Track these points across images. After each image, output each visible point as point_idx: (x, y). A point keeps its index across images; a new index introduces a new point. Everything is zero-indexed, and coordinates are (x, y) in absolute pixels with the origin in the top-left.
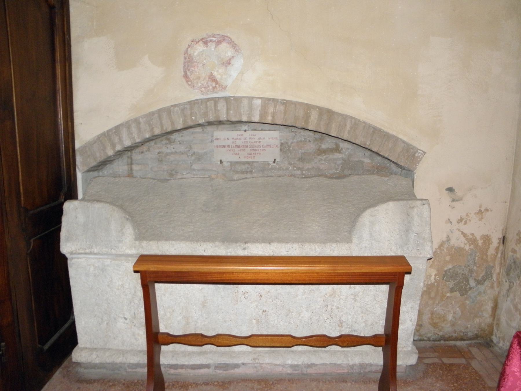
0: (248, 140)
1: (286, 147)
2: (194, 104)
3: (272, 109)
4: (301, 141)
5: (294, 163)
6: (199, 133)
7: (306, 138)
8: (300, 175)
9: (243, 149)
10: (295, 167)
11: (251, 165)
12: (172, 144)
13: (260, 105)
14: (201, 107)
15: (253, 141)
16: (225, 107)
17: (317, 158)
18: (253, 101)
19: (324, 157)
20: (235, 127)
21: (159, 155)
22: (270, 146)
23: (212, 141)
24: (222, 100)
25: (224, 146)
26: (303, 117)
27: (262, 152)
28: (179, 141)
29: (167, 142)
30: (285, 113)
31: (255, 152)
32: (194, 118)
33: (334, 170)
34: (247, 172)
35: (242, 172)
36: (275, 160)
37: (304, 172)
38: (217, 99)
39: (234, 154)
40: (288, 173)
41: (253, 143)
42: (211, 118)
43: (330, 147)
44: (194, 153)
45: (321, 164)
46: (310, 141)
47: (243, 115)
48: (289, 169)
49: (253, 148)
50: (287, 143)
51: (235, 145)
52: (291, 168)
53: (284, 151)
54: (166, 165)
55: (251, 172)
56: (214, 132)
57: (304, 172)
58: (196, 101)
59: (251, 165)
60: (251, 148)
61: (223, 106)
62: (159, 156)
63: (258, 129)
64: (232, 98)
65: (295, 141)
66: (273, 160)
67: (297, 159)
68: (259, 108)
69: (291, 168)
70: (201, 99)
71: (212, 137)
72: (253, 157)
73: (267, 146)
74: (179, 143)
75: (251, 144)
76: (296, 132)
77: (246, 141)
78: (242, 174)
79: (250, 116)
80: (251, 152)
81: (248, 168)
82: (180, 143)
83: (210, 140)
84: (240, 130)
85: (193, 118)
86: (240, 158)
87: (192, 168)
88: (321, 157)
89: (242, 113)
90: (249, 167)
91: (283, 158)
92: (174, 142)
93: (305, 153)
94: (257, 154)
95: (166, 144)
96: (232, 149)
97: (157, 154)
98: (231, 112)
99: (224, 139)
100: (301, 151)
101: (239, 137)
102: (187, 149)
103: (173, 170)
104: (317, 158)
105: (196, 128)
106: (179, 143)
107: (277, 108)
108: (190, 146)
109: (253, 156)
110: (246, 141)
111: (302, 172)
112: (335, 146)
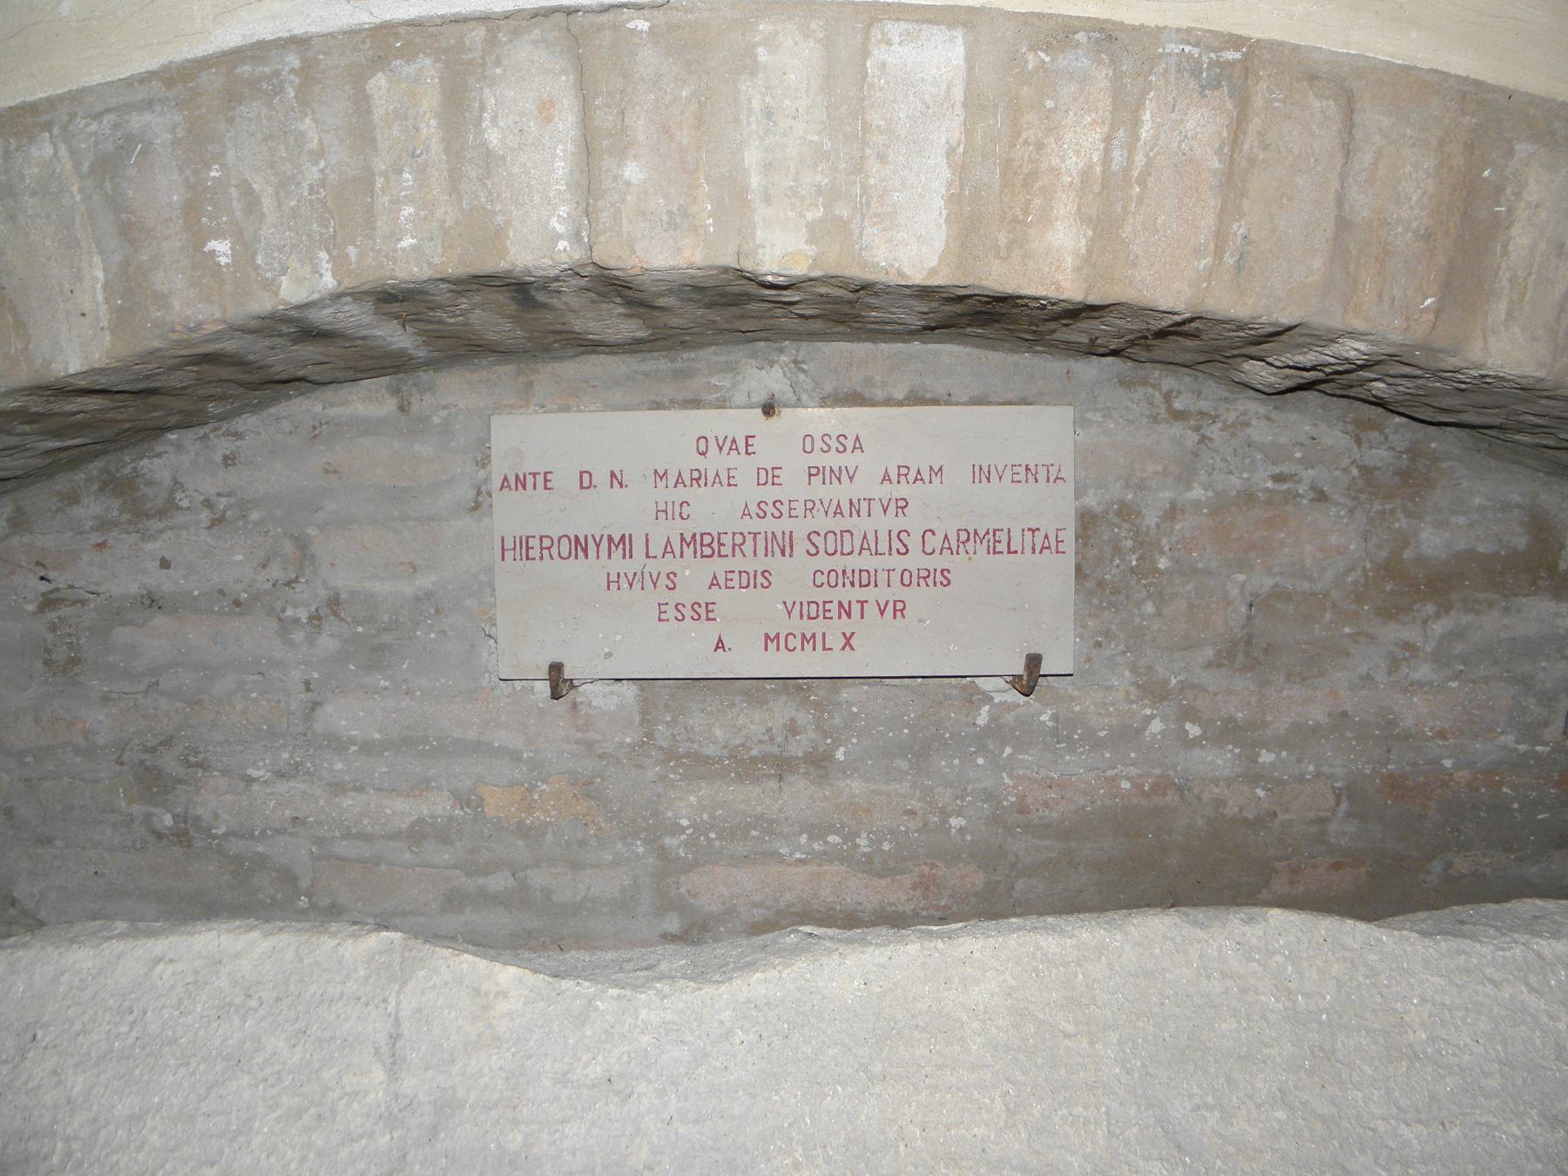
0: (794, 487)
1: (1117, 550)
2: (232, 97)
3: (1097, 135)
4: (1248, 498)
5: (1184, 686)
6: (369, 427)
7: (1285, 468)
8: (1229, 782)
9: (750, 565)
10: (1189, 714)
11: (817, 705)
12: (155, 525)
13: (958, 93)
14: (307, 124)
15: (841, 492)
16: (566, 121)
17: (1372, 638)
18: (878, 53)
19: (1439, 628)
20: (680, 375)
21: (52, 615)
22: (994, 541)
23: (478, 505)
24: (525, 51)
25: (580, 546)
26: (1428, 237)
27: (917, 598)
28: (208, 504)
29: (113, 507)
30: (1232, 182)
31: (858, 593)
32: (222, 248)
33: (1509, 739)
34: (782, 766)
35: (744, 766)
36: (1034, 661)
37: (1266, 757)
38: (479, 34)
39: (671, 613)
40: (1133, 771)
41: (838, 512)
42: (407, 242)
43: (1481, 549)
44: (334, 602)
45: (1410, 687)
46: (1321, 497)
47: (767, 200)
48: (1139, 732)
49: (838, 562)
50: (1126, 512)
51: (673, 529)
52: (1156, 726)
53: (1101, 584)
54: (106, 699)
55: (819, 763)
56: (496, 421)
57: (1266, 757)
58: (245, 70)
59: (817, 705)
60: (823, 562)
61: (546, 110)
62: (53, 628)
63: (880, 394)
64: (643, 25)
65: (1197, 493)
66: (1019, 668)
67: (1209, 653)
68: (950, 129)
69: (1156, 726)
70: (299, 43)
71: (484, 462)
72: (836, 641)
73: (969, 537)
74: (205, 516)
75: (822, 522)
76: (1202, 413)
77: (770, 493)
78: (740, 779)
79: (843, 211)
80: (821, 595)
81: (792, 729)
82: (218, 521)
83: (466, 492)
84: (722, 404)
85: (213, 245)
86: (720, 645)
87: (319, 728)
88: (1411, 634)
89: (755, 181)
90: (803, 718)
91: (1099, 644)
92: (169, 508)
93: (1277, 594)
94: (871, 609)
95: (104, 525)
96: (653, 567)
97: (31, 608)
98: (633, 171)
99: (585, 480)
100: (1241, 578)
101: (715, 462)
102: (275, 572)
103: (168, 742)
104: (1372, 638)
105: (345, 391)
106: (205, 516)
107: (1145, 132)
108: (302, 544)
109: (835, 629)
110: (770, 493)
111: (1253, 759)
112: (1521, 542)
